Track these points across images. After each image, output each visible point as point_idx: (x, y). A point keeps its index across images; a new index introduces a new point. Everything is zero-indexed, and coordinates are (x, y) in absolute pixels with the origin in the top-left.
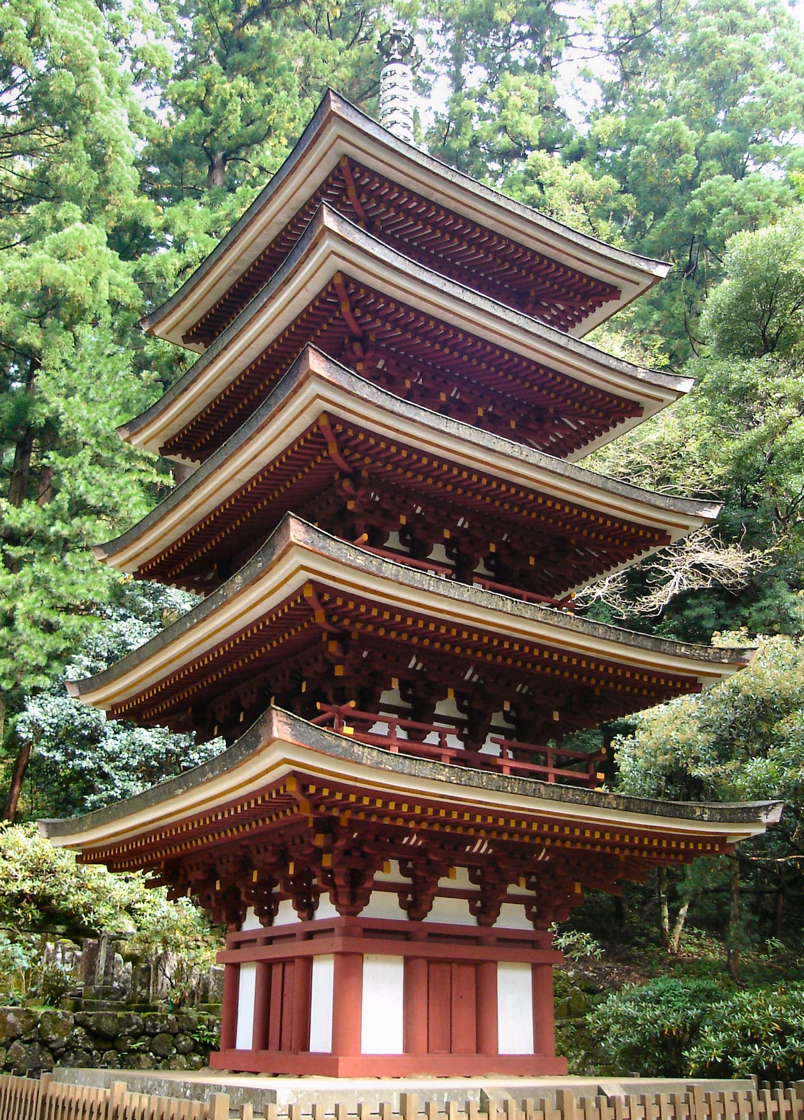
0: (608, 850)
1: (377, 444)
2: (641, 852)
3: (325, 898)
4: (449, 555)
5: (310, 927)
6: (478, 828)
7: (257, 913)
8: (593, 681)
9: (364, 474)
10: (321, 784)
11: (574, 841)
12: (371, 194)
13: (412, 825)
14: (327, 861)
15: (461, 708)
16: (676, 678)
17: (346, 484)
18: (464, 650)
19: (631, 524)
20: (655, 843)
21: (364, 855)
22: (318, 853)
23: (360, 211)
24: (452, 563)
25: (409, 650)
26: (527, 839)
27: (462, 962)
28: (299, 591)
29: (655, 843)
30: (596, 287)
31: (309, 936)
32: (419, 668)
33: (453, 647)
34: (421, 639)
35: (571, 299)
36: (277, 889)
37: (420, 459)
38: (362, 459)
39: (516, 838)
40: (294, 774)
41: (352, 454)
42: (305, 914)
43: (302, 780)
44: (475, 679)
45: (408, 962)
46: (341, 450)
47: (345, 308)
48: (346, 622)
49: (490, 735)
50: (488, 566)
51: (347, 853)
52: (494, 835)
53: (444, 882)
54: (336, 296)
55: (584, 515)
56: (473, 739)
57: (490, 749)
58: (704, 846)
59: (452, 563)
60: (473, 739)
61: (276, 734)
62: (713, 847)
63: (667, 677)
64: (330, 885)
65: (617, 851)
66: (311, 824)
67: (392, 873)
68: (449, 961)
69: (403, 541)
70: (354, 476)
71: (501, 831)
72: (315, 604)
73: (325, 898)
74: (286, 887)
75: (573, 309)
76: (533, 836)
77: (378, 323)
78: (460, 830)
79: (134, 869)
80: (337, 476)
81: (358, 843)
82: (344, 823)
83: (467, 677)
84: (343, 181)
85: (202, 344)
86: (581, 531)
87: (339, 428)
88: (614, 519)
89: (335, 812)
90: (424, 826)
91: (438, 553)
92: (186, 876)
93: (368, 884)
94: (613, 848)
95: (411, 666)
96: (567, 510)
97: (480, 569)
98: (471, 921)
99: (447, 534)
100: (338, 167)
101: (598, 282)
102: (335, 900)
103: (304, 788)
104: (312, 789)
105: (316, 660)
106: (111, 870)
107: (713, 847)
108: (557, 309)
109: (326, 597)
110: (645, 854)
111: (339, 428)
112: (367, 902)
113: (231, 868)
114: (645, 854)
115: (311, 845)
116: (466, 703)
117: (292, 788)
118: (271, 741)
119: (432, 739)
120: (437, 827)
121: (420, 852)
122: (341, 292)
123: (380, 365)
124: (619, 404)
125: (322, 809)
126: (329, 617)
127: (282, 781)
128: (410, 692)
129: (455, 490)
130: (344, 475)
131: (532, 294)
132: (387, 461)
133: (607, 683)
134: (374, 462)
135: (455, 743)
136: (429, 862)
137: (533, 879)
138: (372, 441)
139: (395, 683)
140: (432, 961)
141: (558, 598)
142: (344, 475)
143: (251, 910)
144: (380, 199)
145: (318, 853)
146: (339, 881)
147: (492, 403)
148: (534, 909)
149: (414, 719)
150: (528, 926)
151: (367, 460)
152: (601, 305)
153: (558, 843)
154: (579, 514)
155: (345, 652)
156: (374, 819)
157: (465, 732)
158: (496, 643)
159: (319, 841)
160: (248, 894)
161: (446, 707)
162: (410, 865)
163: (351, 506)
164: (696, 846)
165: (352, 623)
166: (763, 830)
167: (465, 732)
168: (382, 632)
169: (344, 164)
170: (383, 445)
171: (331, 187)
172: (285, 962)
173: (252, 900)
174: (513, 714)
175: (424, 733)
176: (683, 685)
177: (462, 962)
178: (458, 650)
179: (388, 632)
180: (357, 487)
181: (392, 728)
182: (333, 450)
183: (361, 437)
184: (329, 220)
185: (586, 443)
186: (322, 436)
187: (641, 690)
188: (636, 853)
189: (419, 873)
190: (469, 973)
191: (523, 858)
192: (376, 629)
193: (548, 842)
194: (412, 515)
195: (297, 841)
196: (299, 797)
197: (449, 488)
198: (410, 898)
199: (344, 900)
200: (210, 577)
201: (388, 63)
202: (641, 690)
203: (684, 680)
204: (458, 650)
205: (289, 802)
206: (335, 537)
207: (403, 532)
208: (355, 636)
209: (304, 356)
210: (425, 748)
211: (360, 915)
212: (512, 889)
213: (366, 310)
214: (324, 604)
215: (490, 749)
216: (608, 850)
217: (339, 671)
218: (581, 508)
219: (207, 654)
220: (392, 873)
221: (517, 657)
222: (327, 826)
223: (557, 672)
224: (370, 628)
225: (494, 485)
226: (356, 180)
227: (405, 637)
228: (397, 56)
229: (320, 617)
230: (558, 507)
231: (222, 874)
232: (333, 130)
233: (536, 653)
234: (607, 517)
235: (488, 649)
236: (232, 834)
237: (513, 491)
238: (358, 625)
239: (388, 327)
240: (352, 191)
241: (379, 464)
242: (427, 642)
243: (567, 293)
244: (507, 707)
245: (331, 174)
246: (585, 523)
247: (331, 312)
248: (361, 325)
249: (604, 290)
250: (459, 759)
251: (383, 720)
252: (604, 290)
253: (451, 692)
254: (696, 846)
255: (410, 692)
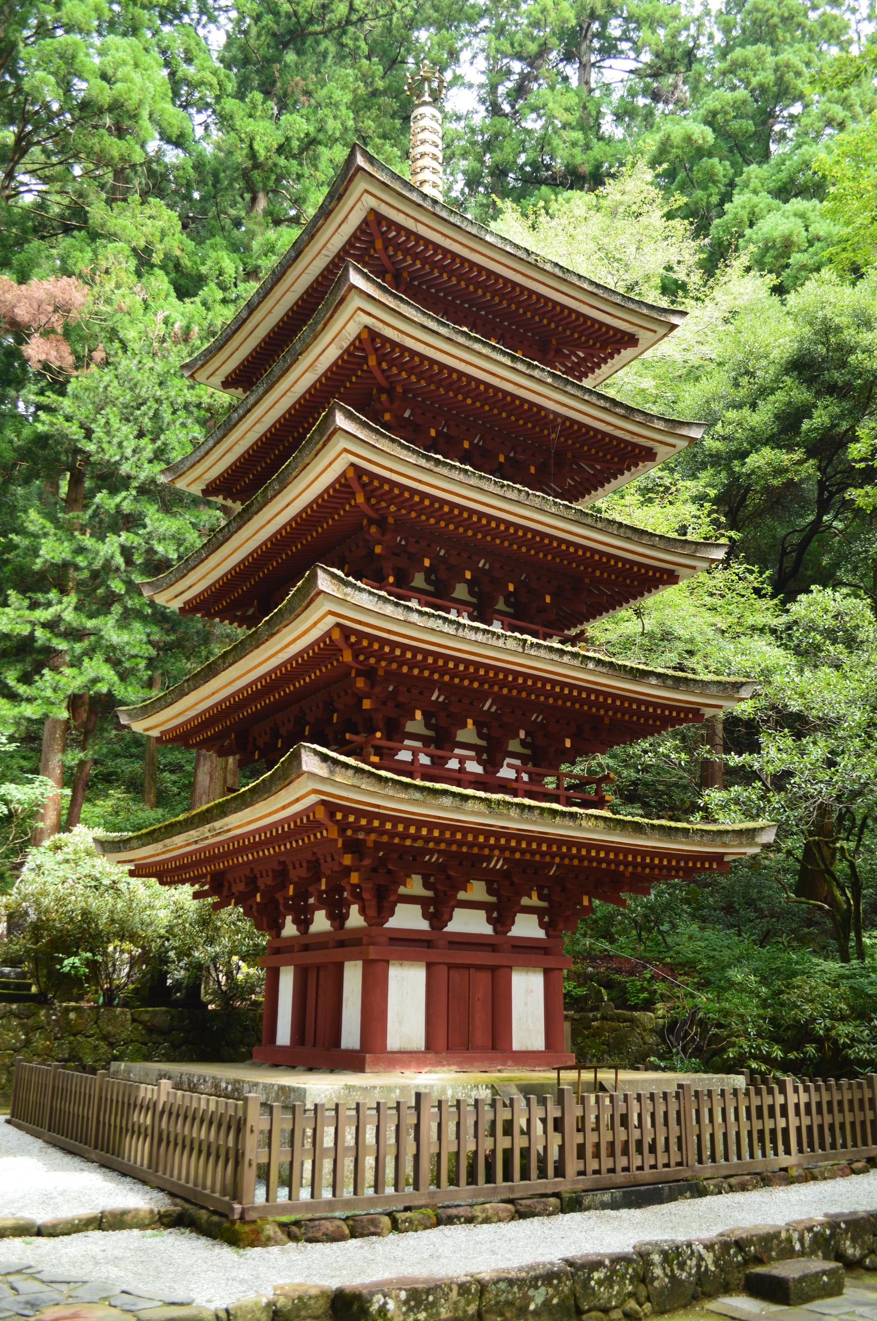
0: (613, 867)
1: (401, 494)
2: (644, 868)
3: (354, 909)
4: (471, 593)
5: (341, 936)
6: (492, 848)
7: (294, 922)
8: (602, 712)
9: (391, 520)
10: (347, 811)
11: (581, 859)
12: (398, 247)
13: (431, 845)
14: (355, 878)
15: (480, 735)
16: (679, 709)
17: (373, 529)
18: (481, 684)
19: (641, 565)
20: (657, 861)
21: (389, 872)
22: (347, 871)
23: (388, 265)
24: (474, 600)
25: (430, 685)
26: (537, 858)
27: (480, 968)
28: (328, 634)
29: (657, 861)
30: (615, 335)
31: (341, 944)
32: (441, 699)
33: (471, 682)
34: (442, 676)
35: (591, 347)
36: (312, 901)
37: (441, 507)
38: (388, 507)
39: (528, 856)
40: (323, 802)
41: (378, 503)
42: (337, 923)
43: (330, 808)
44: (493, 709)
45: (429, 967)
46: (368, 500)
47: (372, 361)
48: (372, 661)
49: (508, 760)
50: (507, 603)
51: (374, 870)
52: (507, 854)
53: (462, 895)
54: (363, 350)
55: (597, 557)
56: (492, 763)
57: (506, 773)
58: (703, 864)
59: (474, 600)
60: (492, 763)
61: (304, 768)
62: (711, 865)
63: (671, 708)
64: (358, 898)
65: (622, 868)
66: (340, 845)
67: (415, 886)
68: (467, 967)
69: (428, 581)
70: (381, 522)
71: (513, 851)
72: (341, 644)
73: (354, 909)
74: (319, 899)
75: (593, 356)
76: (543, 854)
77: (404, 375)
78: (475, 850)
79: (183, 882)
80: (365, 522)
81: (383, 861)
82: (370, 844)
83: (486, 708)
84: (371, 234)
85: (240, 390)
86: (594, 571)
87: (365, 479)
88: (625, 561)
89: (361, 836)
90: (443, 846)
91: (461, 591)
92: (230, 889)
93: (393, 898)
94: (617, 866)
95: (434, 698)
96: (580, 553)
97: (501, 606)
98: (488, 930)
99: (468, 575)
100: (365, 221)
101: (617, 330)
102: (362, 911)
103: (332, 815)
104: (339, 816)
105: (346, 693)
106: (162, 883)
107: (711, 865)
108: (578, 356)
109: (353, 639)
110: (647, 871)
111: (365, 479)
112: (392, 914)
113: (269, 881)
114: (647, 871)
115: (340, 864)
116: (485, 731)
117: (321, 814)
118: (300, 774)
119: (453, 764)
120: (454, 848)
121: (441, 868)
122: (368, 346)
123: (407, 414)
124: (633, 450)
125: (349, 833)
126: (355, 656)
127: (312, 808)
128: (433, 721)
129: (475, 534)
130: (371, 521)
131: (554, 342)
132: (411, 509)
133: (615, 713)
134: (399, 510)
135: (473, 767)
136: (449, 877)
137: (546, 891)
138: (396, 491)
139: (418, 715)
140: (450, 966)
141: (573, 632)
142: (371, 521)
143: (289, 919)
144: (407, 252)
145: (347, 871)
146: (366, 896)
147: (513, 449)
148: (546, 919)
149: (437, 748)
150: (541, 934)
151: (393, 508)
152: (619, 353)
153: (567, 861)
154: (592, 556)
155: (373, 686)
156: (396, 841)
157: (485, 757)
158: (510, 678)
159: (347, 860)
160: (286, 906)
161: (468, 733)
162: (432, 879)
163: (378, 549)
164: (695, 864)
165: (378, 662)
166: (757, 850)
167: (485, 757)
168: (405, 669)
169: (372, 218)
170: (407, 495)
171: (358, 240)
172: (318, 968)
173: (290, 910)
174: (529, 740)
175: (446, 760)
176: (686, 715)
177: (480, 968)
178: (476, 685)
179: (411, 669)
180: (383, 533)
181: (415, 755)
182: (360, 499)
183: (386, 487)
184: (355, 279)
185: (603, 486)
186: (349, 487)
187: (646, 720)
188: (639, 870)
189: (439, 887)
190: (483, 979)
191: (536, 873)
192: (400, 666)
193: (557, 860)
194: (435, 558)
195: (329, 859)
196: (327, 822)
197: (470, 533)
198: (432, 909)
199: (372, 912)
200: (250, 612)
201: (418, 106)
202: (646, 720)
203: (687, 711)
204: (476, 685)
205: (316, 825)
206: (359, 583)
207: (428, 572)
208: (381, 672)
209: (330, 416)
210: (446, 774)
211: (386, 925)
212: (525, 901)
213: (392, 363)
214: (352, 646)
215: (506, 773)
216: (613, 867)
217: (367, 704)
218: (594, 551)
219: (245, 688)
220: (415, 886)
221: (530, 690)
222: (353, 846)
223: (569, 704)
224: (394, 666)
225: (512, 530)
226: (383, 233)
227: (426, 673)
228: (427, 98)
229: (347, 657)
230: (572, 550)
231: (263, 887)
232: (360, 185)
233: (548, 687)
234: (618, 558)
235: (503, 684)
236: (270, 852)
237: (529, 536)
238: (383, 664)
239: (413, 378)
240: (379, 244)
241: (403, 512)
242: (447, 678)
243: (587, 341)
244: (522, 734)
245: (359, 228)
246: (598, 565)
247: (360, 365)
248: (388, 377)
249: (622, 338)
250: (478, 783)
251: (408, 748)
252: (622, 338)
253: (470, 722)
254: (695, 864)
255: (433, 721)
